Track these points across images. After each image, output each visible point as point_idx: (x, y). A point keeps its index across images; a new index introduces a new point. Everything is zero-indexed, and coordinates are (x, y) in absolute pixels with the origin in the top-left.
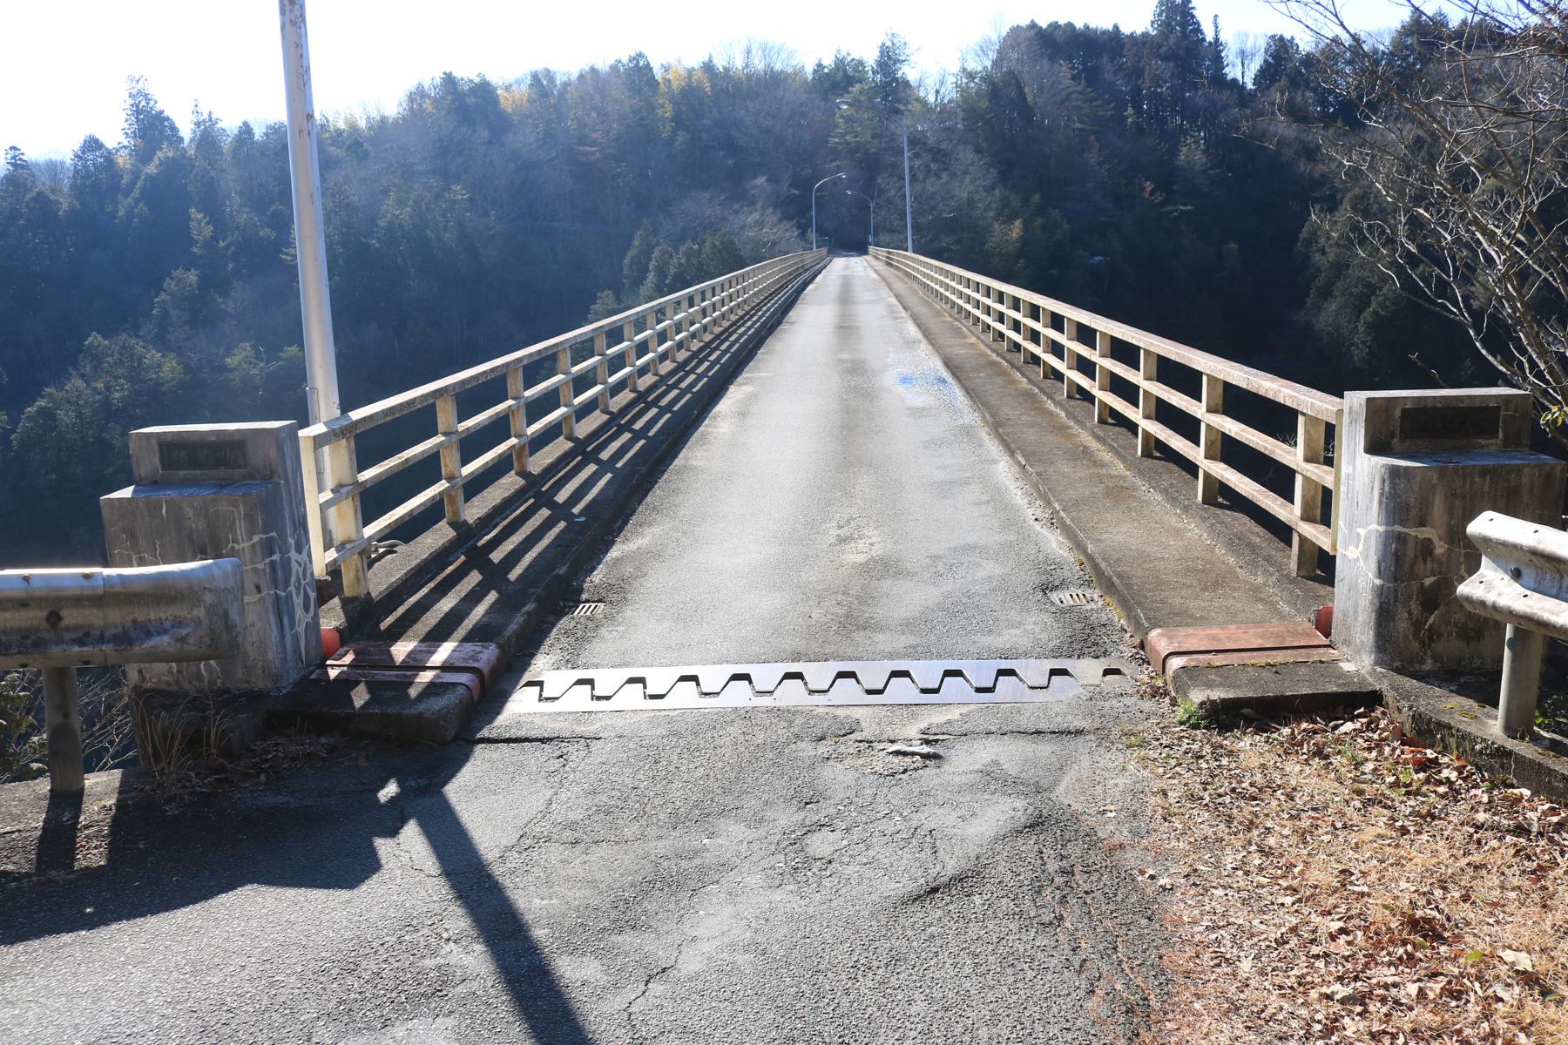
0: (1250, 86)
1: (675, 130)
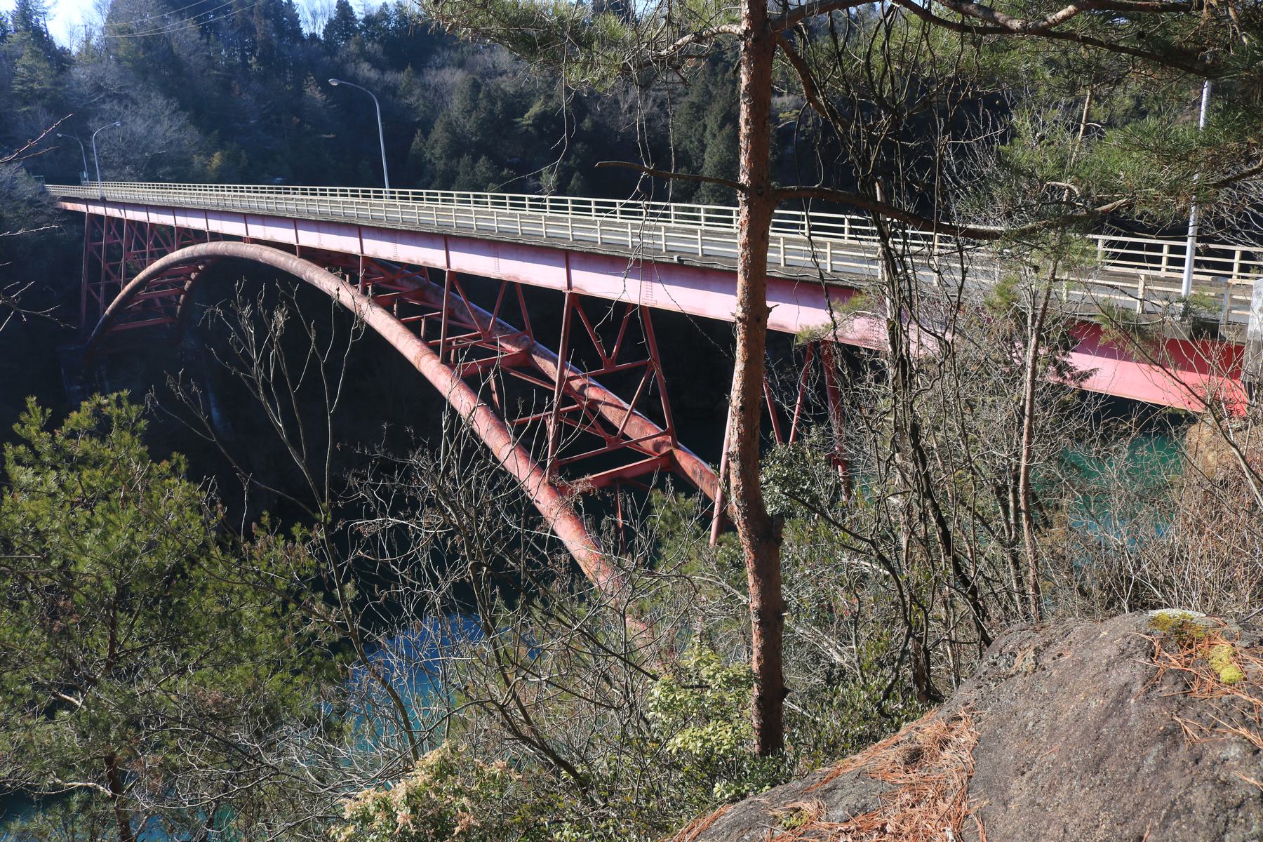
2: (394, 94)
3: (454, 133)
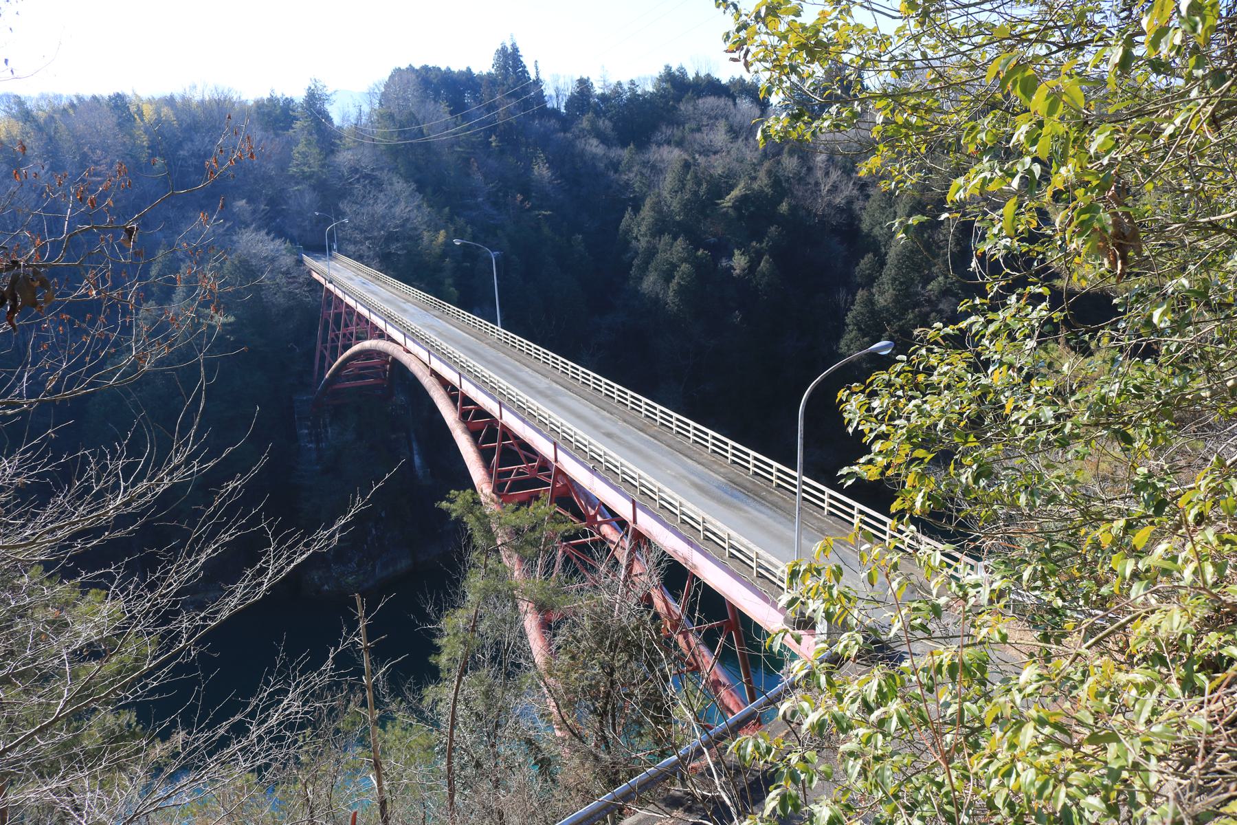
0: (563, 110)
1: (152, 155)
2: (616, 171)
3: (660, 212)
